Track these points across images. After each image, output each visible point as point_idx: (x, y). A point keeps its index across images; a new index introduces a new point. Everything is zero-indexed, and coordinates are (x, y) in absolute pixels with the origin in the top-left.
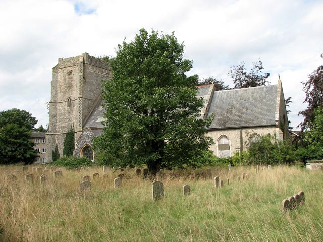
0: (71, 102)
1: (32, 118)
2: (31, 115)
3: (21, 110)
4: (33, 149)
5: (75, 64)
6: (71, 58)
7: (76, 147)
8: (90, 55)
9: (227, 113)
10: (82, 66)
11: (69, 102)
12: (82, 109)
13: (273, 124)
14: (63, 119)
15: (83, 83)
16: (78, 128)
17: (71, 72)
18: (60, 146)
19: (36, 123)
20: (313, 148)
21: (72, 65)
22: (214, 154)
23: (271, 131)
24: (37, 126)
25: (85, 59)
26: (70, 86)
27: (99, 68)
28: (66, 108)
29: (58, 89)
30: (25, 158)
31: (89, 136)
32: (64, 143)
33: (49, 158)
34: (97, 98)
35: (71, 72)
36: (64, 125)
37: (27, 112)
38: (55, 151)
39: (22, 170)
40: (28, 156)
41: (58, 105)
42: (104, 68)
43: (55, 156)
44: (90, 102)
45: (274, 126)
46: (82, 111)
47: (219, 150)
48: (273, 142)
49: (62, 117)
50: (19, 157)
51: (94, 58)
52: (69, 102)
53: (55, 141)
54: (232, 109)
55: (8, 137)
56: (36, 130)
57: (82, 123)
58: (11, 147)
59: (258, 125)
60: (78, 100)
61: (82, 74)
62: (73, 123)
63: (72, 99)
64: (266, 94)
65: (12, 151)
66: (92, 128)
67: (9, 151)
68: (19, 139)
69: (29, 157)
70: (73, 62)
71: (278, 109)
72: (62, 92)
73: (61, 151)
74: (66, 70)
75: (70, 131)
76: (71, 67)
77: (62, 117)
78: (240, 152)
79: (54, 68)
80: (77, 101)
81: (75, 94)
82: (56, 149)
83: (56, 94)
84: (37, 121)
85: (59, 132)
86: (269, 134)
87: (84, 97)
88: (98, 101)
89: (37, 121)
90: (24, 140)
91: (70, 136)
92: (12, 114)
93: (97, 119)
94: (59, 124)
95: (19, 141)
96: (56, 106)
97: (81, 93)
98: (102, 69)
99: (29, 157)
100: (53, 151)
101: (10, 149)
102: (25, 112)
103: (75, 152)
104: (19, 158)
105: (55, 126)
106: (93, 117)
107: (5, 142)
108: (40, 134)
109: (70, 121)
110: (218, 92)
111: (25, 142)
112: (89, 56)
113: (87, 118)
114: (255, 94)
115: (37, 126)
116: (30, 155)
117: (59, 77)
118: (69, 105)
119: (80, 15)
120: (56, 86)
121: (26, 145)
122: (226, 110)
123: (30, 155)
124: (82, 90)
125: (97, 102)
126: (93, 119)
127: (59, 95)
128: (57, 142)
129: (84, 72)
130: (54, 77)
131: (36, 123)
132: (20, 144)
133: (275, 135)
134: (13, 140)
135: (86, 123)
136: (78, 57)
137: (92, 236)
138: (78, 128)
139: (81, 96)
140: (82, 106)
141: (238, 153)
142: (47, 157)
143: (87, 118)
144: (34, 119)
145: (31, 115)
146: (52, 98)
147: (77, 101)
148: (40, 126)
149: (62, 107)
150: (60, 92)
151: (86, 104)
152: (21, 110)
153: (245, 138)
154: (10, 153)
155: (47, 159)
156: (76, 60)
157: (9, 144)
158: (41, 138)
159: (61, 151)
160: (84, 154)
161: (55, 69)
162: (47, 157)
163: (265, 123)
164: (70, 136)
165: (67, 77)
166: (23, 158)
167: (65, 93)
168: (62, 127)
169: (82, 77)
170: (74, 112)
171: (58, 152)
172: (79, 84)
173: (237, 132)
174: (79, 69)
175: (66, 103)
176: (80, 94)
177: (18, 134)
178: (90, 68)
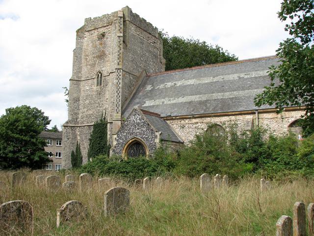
0: (103, 78)
1: (45, 117)
2: (43, 113)
3: (32, 107)
4: (44, 150)
5: (110, 24)
6: (104, 16)
7: (115, 143)
8: (133, 12)
10: (122, 23)
11: (100, 78)
12: (120, 86)
14: (90, 103)
15: (123, 48)
16: (114, 117)
17: (103, 35)
18: (83, 144)
19: (49, 124)
21: (106, 25)
24: (49, 127)
26: (102, 56)
27: (145, 33)
28: (95, 88)
29: (83, 61)
30: (31, 160)
31: (138, 124)
32: (90, 140)
33: (67, 162)
35: (103, 35)
36: (91, 112)
37: (39, 109)
38: (77, 152)
39: (11, 179)
40: (36, 158)
41: (82, 83)
42: (150, 34)
43: (76, 159)
44: (131, 78)
46: (120, 90)
49: (88, 101)
50: (23, 160)
51: (138, 16)
52: (100, 78)
53: (76, 137)
55: (10, 132)
56: (49, 130)
57: (120, 108)
58: (14, 146)
60: (115, 74)
61: (122, 35)
62: (105, 109)
63: (105, 73)
65: (14, 152)
66: (145, 112)
67: (10, 152)
68: (25, 135)
69: (38, 159)
70: (108, 21)
72: (90, 65)
73: (84, 152)
74: (96, 34)
75: (99, 122)
76: (105, 28)
77: (88, 101)
79: (78, 31)
80: (114, 76)
81: (110, 65)
82: (78, 148)
83: (80, 68)
84: (50, 121)
85: (82, 123)
87: (124, 69)
88: (143, 78)
89: (50, 121)
90: (32, 137)
91: (100, 129)
92: (21, 111)
93: (145, 103)
94: (83, 112)
95: (27, 138)
96: (79, 85)
97: (120, 63)
98: (148, 35)
99: (38, 159)
100: (73, 152)
101: (11, 149)
102: (37, 110)
103: (114, 151)
104: (22, 162)
105: (76, 114)
106: (137, 100)
107: (8, 139)
108: (54, 135)
109: (99, 105)
111: (34, 140)
112: (131, 11)
113: (128, 101)
115: (49, 127)
116: (40, 157)
117: (85, 44)
118: (99, 83)
120: (81, 57)
121: (34, 144)
123: (40, 157)
124: (122, 58)
125: (141, 79)
126: (138, 103)
127: (85, 70)
128: (79, 138)
129: (124, 32)
130: (77, 43)
131: (48, 123)
132: (26, 143)
134: (17, 136)
135: (126, 109)
136: (117, 12)
138: (114, 117)
139: (120, 67)
140: (121, 81)
142: (63, 162)
143: (128, 101)
144: (47, 118)
145: (43, 113)
146: (74, 73)
147: (114, 76)
148: (53, 126)
149: (89, 87)
150: (87, 65)
151: (127, 81)
152: (32, 107)
154: (10, 155)
155: (63, 163)
156: (112, 17)
157: (11, 141)
158: (54, 139)
159: (84, 152)
160: (129, 154)
161: (80, 32)
162: (63, 162)
164: (100, 129)
165: (98, 43)
166: (28, 162)
167: (93, 65)
168: (88, 116)
169: (122, 39)
170: (107, 93)
171: (80, 153)
172: (117, 49)
174: (118, 28)
175: (96, 80)
176: (118, 64)
177: (24, 128)
178: (132, 29)
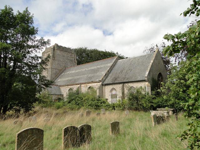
8: (59, 45)
9: (119, 73)
13: (144, 79)
20: (165, 97)
22: (108, 101)
23: (143, 85)
25: (55, 47)
34: (63, 68)
45: (144, 81)
47: (111, 98)
48: (143, 93)
51: (61, 46)
54: (123, 70)
59: (135, 80)
64: (146, 59)
71: (149, 69)
78: (121, 100)
86: (141, 87)
98: (68, 53)
110: (119, 60)
112: (58, 45)
114: (140, 60)
119: (106, 36)
122: (119, 72)
125: (62, 70)
133: (145, 88)
137: (105, 135)
141: (120, 101)
153: (126, 91)
163: (139, 79)
173: (121, 85)
178: (58, 52)
